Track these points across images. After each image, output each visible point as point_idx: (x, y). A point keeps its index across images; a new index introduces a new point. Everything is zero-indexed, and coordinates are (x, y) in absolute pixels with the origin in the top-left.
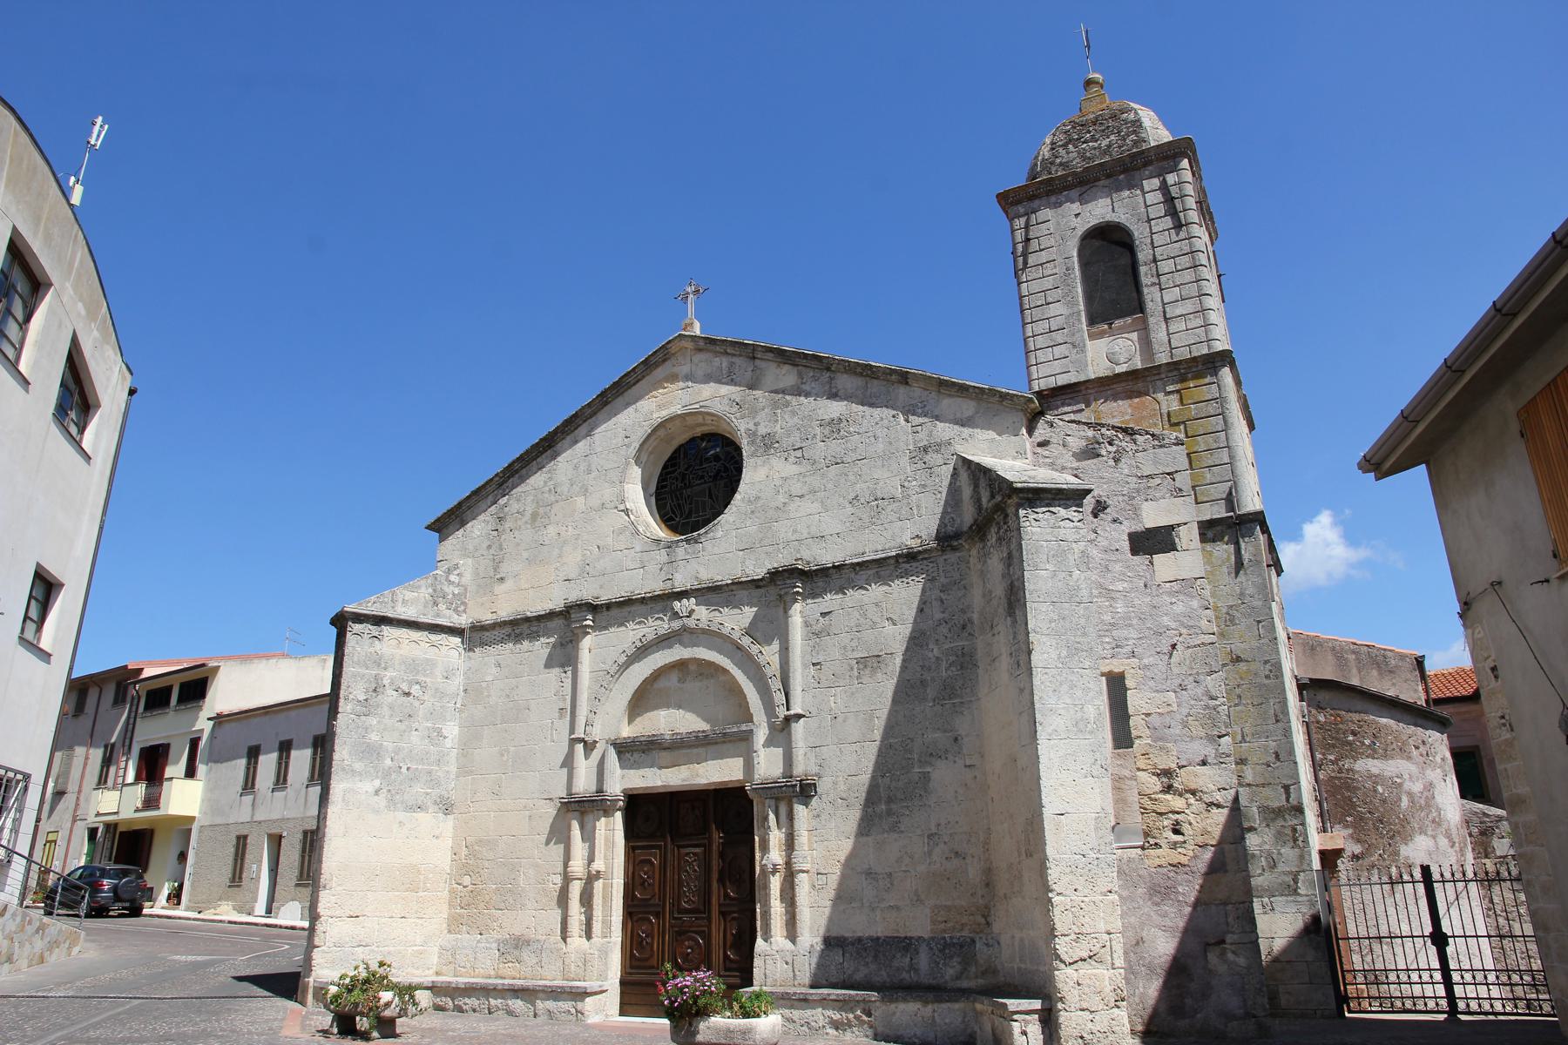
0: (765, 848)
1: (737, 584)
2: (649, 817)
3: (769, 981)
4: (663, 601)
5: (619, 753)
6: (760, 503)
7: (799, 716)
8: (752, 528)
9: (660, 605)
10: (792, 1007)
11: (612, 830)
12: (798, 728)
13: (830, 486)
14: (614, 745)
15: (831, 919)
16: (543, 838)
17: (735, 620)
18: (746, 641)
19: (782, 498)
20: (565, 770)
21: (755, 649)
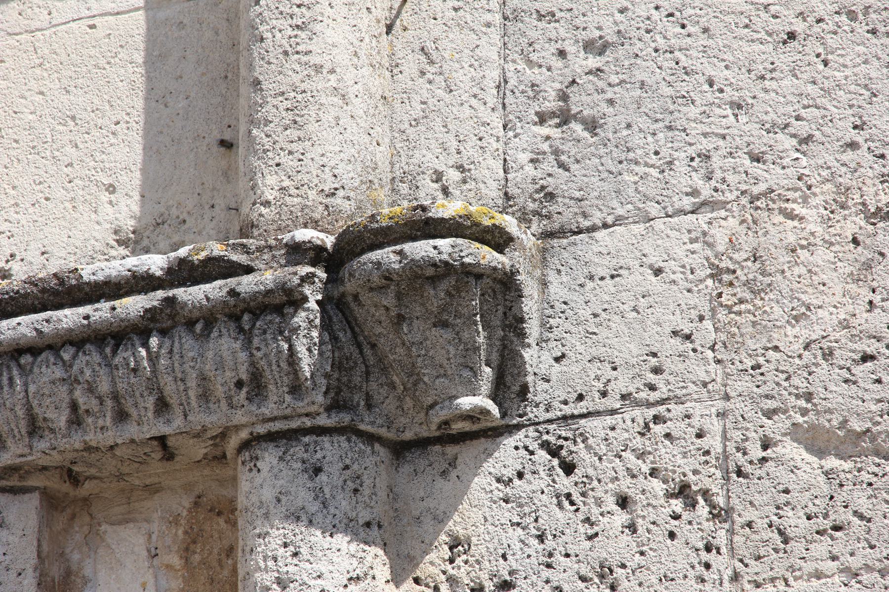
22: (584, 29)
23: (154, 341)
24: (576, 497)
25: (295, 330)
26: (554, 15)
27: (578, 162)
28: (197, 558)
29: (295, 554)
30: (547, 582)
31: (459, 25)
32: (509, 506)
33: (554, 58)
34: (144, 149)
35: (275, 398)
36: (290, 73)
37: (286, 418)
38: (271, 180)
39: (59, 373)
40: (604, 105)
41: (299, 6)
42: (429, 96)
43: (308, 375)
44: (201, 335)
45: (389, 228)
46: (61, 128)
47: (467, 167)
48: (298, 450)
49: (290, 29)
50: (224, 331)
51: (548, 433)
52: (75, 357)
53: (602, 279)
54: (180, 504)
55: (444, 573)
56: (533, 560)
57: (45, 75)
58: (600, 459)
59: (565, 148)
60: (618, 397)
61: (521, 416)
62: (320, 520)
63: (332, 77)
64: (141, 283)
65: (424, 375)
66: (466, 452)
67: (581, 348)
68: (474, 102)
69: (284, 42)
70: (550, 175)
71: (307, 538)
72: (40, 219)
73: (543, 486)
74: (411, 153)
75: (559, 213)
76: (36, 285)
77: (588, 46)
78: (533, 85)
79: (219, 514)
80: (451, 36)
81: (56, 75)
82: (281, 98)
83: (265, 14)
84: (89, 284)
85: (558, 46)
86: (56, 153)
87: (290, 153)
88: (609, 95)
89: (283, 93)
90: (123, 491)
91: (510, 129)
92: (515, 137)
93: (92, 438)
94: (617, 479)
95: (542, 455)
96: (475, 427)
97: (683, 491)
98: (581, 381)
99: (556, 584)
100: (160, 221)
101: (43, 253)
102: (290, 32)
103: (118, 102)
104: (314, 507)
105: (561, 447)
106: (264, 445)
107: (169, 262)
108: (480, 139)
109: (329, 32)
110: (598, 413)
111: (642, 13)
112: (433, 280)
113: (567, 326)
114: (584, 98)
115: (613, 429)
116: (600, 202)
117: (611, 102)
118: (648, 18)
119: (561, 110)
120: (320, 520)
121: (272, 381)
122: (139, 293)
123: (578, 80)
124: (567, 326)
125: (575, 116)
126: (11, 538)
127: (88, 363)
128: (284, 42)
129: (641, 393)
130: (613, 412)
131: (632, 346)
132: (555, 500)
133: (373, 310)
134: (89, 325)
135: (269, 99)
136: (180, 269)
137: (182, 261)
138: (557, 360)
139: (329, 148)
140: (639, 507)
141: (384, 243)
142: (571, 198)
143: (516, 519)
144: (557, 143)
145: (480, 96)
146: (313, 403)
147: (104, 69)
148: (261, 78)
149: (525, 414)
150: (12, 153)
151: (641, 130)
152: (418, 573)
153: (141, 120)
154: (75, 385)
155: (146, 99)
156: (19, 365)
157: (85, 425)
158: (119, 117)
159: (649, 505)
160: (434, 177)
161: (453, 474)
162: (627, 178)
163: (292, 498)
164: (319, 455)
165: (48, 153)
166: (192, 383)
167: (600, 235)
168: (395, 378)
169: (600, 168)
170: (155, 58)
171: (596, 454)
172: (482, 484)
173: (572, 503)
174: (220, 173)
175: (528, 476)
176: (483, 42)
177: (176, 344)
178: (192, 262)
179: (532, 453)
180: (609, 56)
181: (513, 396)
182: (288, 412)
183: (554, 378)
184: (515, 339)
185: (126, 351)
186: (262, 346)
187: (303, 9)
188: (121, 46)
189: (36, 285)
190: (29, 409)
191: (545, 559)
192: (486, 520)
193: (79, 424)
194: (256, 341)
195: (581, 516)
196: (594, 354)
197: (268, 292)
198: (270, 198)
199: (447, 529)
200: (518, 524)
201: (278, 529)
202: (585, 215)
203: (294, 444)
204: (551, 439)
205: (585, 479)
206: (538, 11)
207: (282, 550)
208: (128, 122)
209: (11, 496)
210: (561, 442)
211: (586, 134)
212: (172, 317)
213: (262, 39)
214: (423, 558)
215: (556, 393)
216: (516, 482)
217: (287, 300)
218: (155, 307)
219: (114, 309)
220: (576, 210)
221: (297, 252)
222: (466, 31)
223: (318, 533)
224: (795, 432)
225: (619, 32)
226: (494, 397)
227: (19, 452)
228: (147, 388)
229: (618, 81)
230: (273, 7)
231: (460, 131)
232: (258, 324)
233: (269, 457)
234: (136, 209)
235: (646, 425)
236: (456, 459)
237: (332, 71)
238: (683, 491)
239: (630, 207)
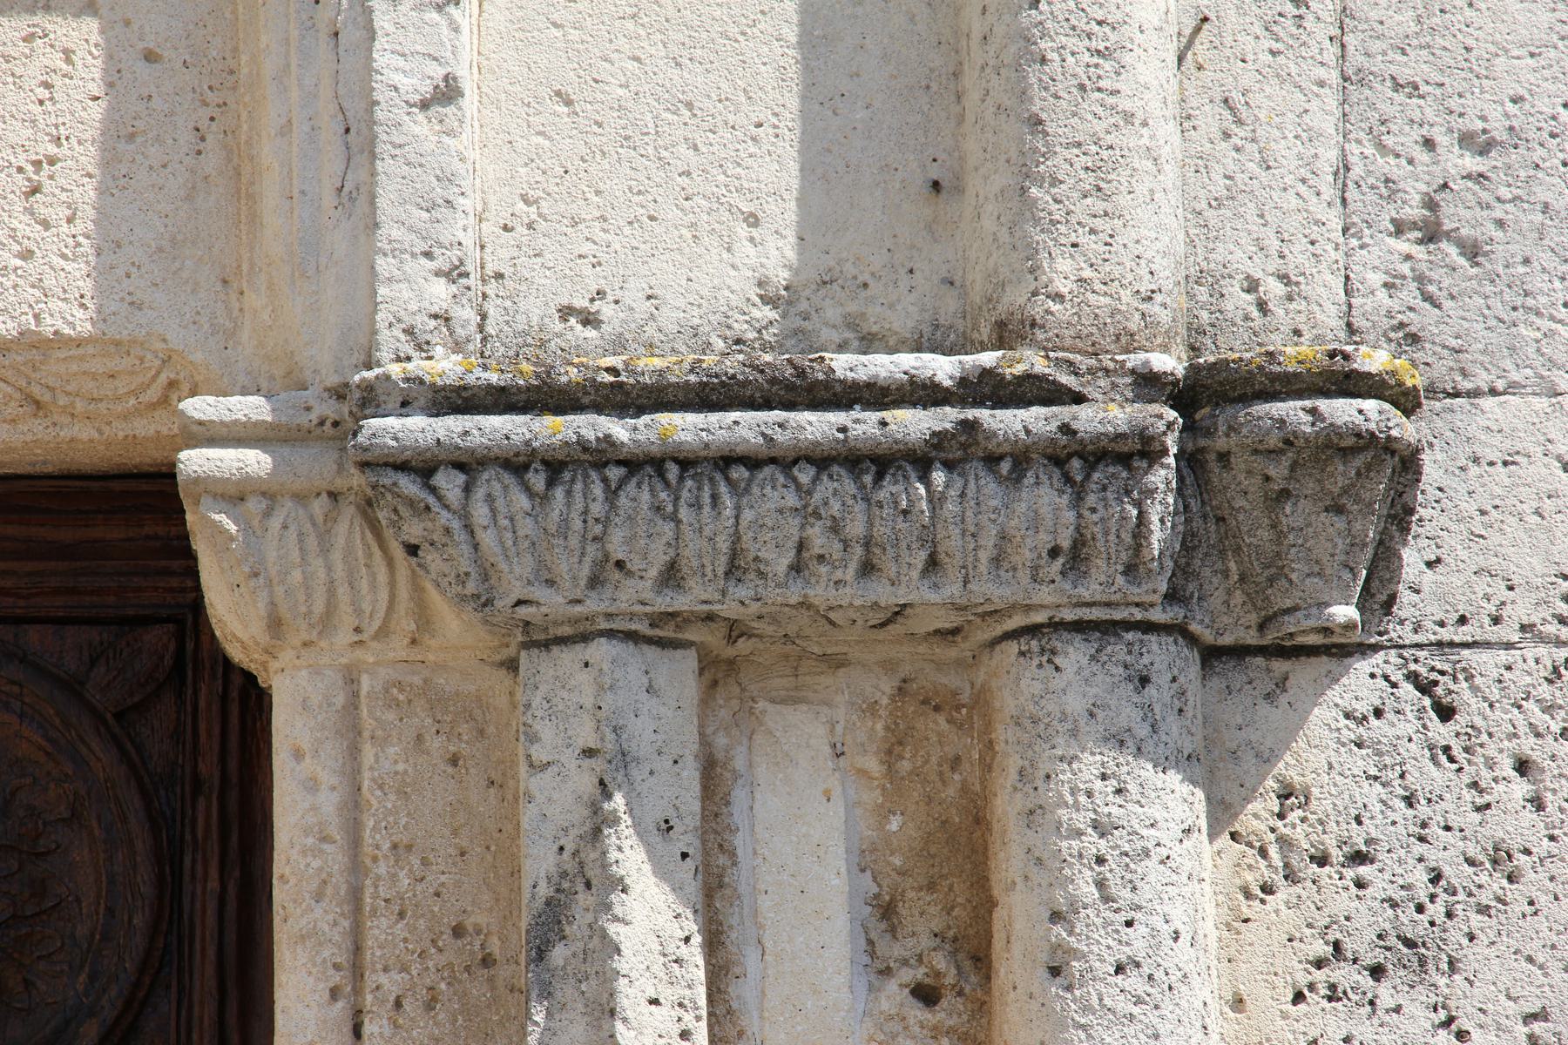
22: (1461, 115)
23: (939, 477)
24: (1457, 751)
25: (1151, 492)
26: (1416, 88)
27: (1453, 297)
28: (905, 766)
29: (1119, 791)
30: (1420, 860)
31: (1278, 76)
32: (1364, 752)
33: (1418, 148)
34: (801, 170)
35: (1103, 578)
36: (1090, 117)
37: (1108, 605)
38: (1064, 265)
39: (792, 500)
40: (1492, 226)
41: (1100, 23)
42: (1236, 169)
43: (1156, 553)
44: (1007, 479)
45: (1296, 375)
46: (670, 116)
47: (1294, 278)
48: (1117, 650)
49: (1087, 54)
50: (1043, 478)
51: (1416, 661)
52: (816, 480)
53: (1491, 464)
54: (877, 687)
55: (1273, 830)
56: (1400, 829)
57: (642, 33)
58: (1491, 706)
59: (1433, 275)
60: (1517, 627)
61: (1380, 634)
62: (1151, 749)
63: (1144, 131)
64: (924, 394)
65: (1293, 570)
66: (1302, 672)
67: (1463, 554)
68: (1302, 189)
69: (1080, 71)
70: (1411, 309)
71: (1136, 771)
72: (642, 246)
73: (1410, 731)
74: (1211, 245)
75: (1427, 364)
76: (762, 372)
77: (1466, 140)
78: (1387, 181)
79: (937, 709)
80: (1268, 90)
81: (659, 36)
82: (1076, 151)
83: (1049, 24)
84: (842, 382)
85: (1425, 131)
86: (664, 153)
87: (1092, 231)
88: (1498, 214)
89: (1079, 145)
90: (786, 657)
91: (1353, 236)
92: (1362, 247)
93: (820, 594)
94: (1515, 735)
95: (1407, 690)
96: (1328, 641)
98: (1464, 599)
99: (1433, 864)
100: (827, 279)
101: (649, 297)
102: (1086, 57)
103: (760, 93)
104: (1143, 731)
105: (1436, 683)
106: (1065, 635)
107: (963, 369)
108: (1312, 243)
109: (1140, 67)
110: (1488, 645)
111: (1545, 109)
112: (1346, 453)
113: (1443, 520)
114: (1462, 212)
115: (1509, 668)
116: (1486, 359)
117: (1500, 224)
118: (1554, 118)
119: (1425, 220)
120: (1151, 749)
121: (1104, 556)
122: (914, 405)
123: (1451, 184)
124: (1443, 520)
125: (1448, 234)
126: (663, 710)
127: (835, 491)
128: (1080, 71)
129: (1548, 627)
130: (1509, 646)
131: (1534, 561)
132: (1427, 753)
133: (1242, 477)
134: (846, 440)
135: (1058, 149)
136: (980, 382)
137: (986, 373)
138: (1429, 564)
139: (1144, 232)
140: (1547, 776)
141: (1281, 393)
142: (1444, 347)
143: (1373, 771)
144: (1424, 267)
145: (1311, 182)
146: (1155, 592)
147: (736, 41)
148: (1044, 116)
149: (1386, 632)
150: (592, 139)
151: (1544, 270)
152: (1237, 827)
153: (797, 125)
154: (812, 520)
155: (804, 98)
156: (727, 479)
157: (807, 572)
158: (762, 117)
159: (1561, 775)
160: (1246, 284)
161: (1283, 699)
162: (1525, 333)
163: (1111, 714)
164: (1146, 660)
165: (650, 150)
166: (989, 540)
167: (1488, 403)
168: (1232, 565)
169: (1486, 312)
171: (1485, 699)
172: (1323, 717)
173: (1452, 760)
174: (922, 225)
175: (1390, 716)
176: (1314, 105)
177: (972, 485)
178: (1003, 376)
179: (1394, 685)
180: (1495, 158)
181: (1376, 607)
182: (1114, 598)
183: (1426, 589)
184: (1397, 534)
185: (896, 482)
186: (1100, 507)
187: (1107, 29)
188: (762, 12)
189: (762, 372)
190: (737, 538)
191: (1418, 830)
192: (1331, 766)
193: (798, 572)
194: (1091, 500)
195: (1467, 780)
196: (1483, 564)
197: (1120, 436)
198: (1064, 291)
199: (1275, 771)
200: (1376, 778)
201: (1093, 754)
202: (1464, 373)
203: (1112, 640)
204: (1423, 671)
205: (1469, 730)
206: (1393, 78)
207: (1099, 784)
208: (775, 127)
209: (631, 645)
210: (1434, 676)
211: (1462, 261)
212: (964, 447)
213: (1043, 60)
214: (1244, 807)
215: (1429, 610)
216: (1373, 721)
217: (1134, 452)
218: (947, 431)
219: (884, 424)
220: (1452, 364)
221: (1148, 384)
222: (1287, 86)
223: (1149, 766)
225: (1511, 128)
226: (1361, 607)
227: (704, 597)
228: (919, 538)
229: (1510, 196)
230: (1061, 18)
231: (1284, 226)
232: (1096, 476)
233: (1074, 654)
234: (791, 255)
235: (1556, 670)
236: (1286, 679)
237: (1145, 124)
239: (1528, 371)
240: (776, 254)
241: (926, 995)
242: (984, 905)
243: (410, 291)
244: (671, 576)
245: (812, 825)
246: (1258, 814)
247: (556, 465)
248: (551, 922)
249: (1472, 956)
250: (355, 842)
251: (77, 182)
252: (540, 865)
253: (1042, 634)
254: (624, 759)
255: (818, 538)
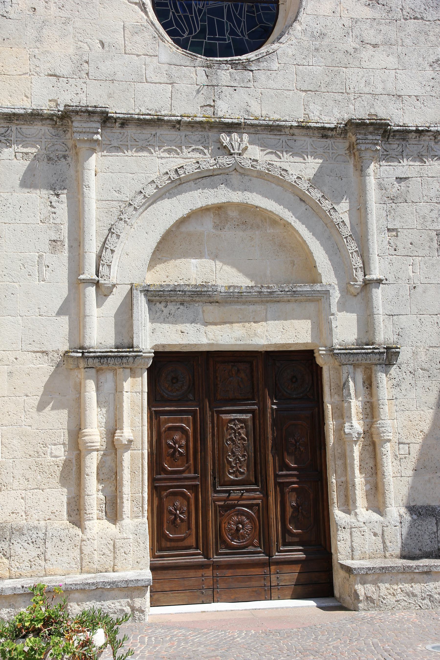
0: (342, 415)
1: (304, 127)
2: (177, 378)
3: (357, 554)
4: (212, 129)
5: (149, 302)
6: (326, 41)
7: (379, 282)
8: (317, 69)
9: (197, 135)
10: (412, 581)
11: (135, 391)
12: (378, 294)
13: (408, 41)
14: (146, 291)
15: (413, 488)
16: (35, 401)
17: (302, 168)
18: (316, 194)
19: (351, 43)
20: (65, 320)
21: (326, 205)
64: (370, 349)
66: (391, 366)
97: (410, 372)
127: (364, 355)
170: (358, 321)
217: (383, 353)
221: (384, 348)
224: (420, 368)
233: (378, 366)
238: (410, 372)
240: (356, 337)
241: (367, 388)
242: (371, 382)
243: (335, 341)
244: (353, 361)
245: (360, 377)
246: (388, 376)
247: (346, 354)
248: (344, 384)
249: (402, 385)
250: (330, 378)
251: (310, 332)
252: (344, 380)
253: (376, 364)
254: (350, 373)
255: (363, 358)
